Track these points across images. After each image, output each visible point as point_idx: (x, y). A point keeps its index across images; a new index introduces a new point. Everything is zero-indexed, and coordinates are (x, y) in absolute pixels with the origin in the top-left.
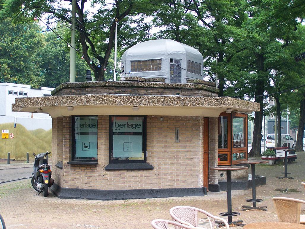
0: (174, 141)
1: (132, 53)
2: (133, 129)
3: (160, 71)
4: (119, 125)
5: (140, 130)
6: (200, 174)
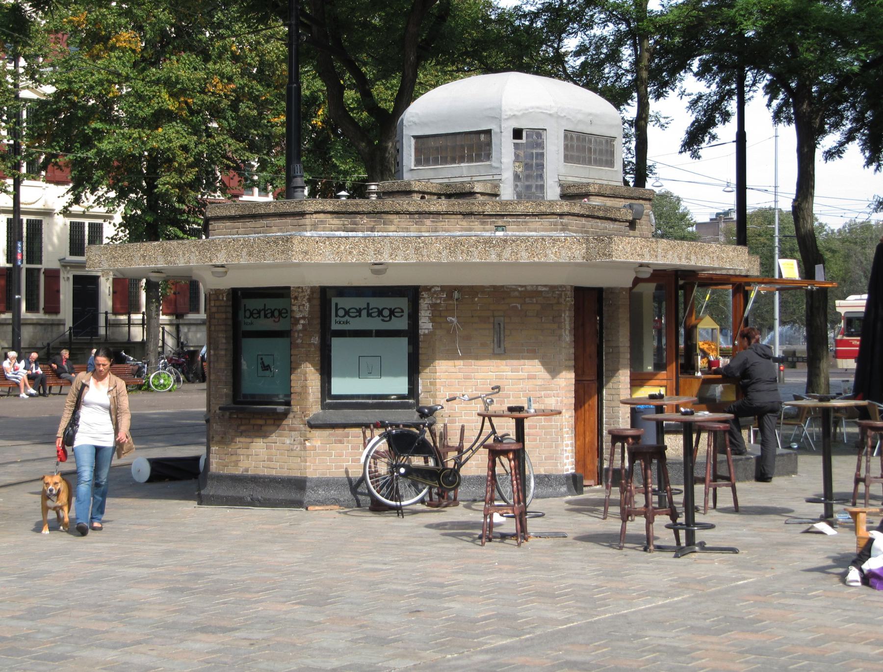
0: (491, 351)
1: (417, 114)
2: (383, 320)
3: (488, 163)
4: (347, 313)
5: (401, 323)
6: (562, 438)
